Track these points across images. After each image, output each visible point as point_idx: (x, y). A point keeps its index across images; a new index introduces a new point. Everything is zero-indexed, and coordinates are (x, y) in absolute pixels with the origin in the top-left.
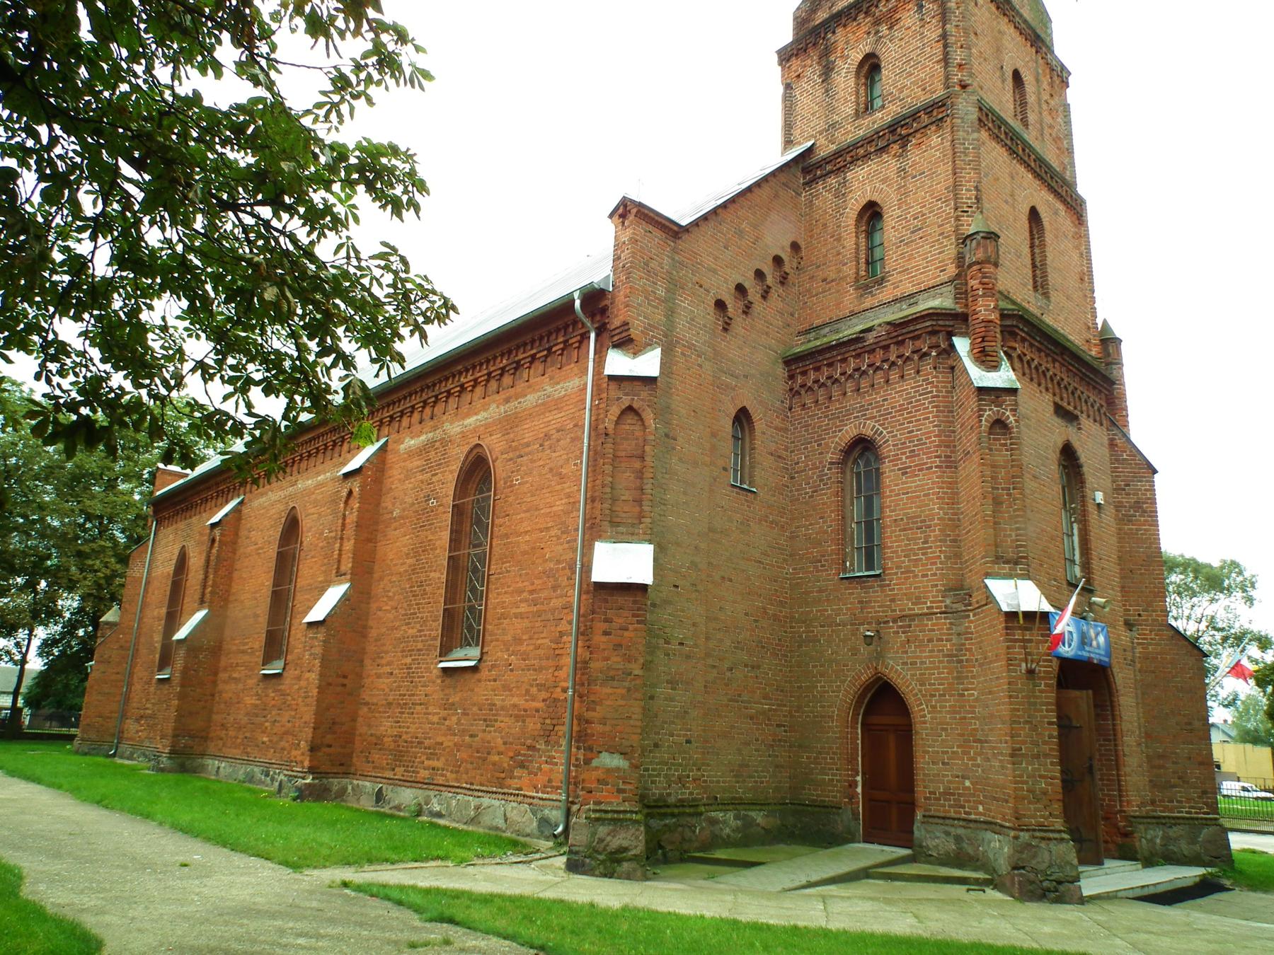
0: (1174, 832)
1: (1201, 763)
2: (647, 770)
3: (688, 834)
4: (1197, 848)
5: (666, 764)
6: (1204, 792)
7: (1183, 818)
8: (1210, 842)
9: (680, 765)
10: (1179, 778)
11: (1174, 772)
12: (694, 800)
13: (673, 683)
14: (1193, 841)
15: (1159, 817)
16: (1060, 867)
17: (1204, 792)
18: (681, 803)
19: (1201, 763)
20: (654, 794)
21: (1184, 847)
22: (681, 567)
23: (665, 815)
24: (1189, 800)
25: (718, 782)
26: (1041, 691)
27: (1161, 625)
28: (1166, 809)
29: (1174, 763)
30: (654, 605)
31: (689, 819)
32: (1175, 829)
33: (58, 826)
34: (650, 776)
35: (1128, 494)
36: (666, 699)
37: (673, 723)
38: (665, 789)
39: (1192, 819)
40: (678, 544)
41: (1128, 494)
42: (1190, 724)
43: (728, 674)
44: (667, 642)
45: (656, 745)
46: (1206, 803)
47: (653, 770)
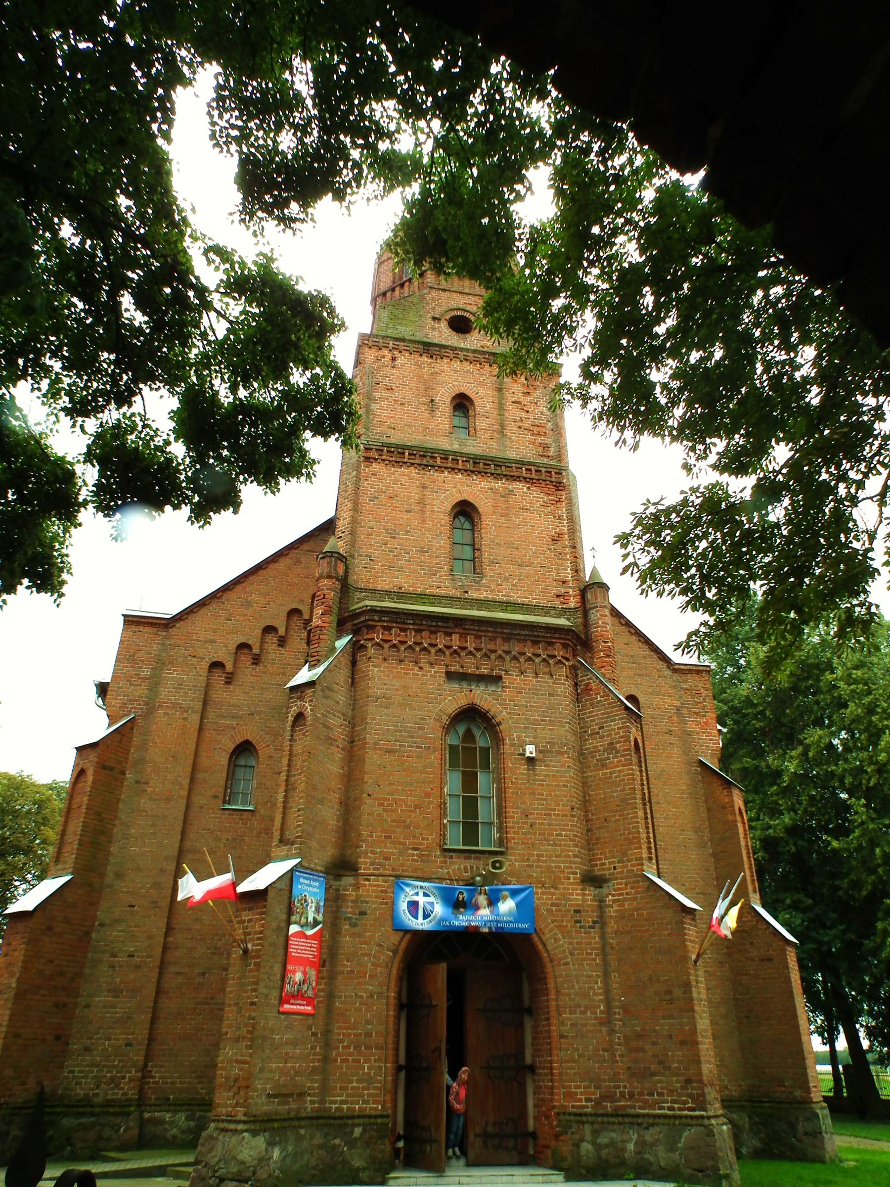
0: (649, 1136)
1: (683, 1043)
2: (73, 1072)
3: (107, 1132)
4: (676, 1156)
5: (97, 1066)
6: (688, 1081)
7: (665, 1116)
8: (692, 1148)
9: (115, 1067)
10: (660, 1062)
11: (654, 1056)
12: (126, 1100)
13: (115, 992)
14: (672, 1147)
15: (637, 1116)
16: (226, 1162)
17: (688, 1081)
18: (109, 1103)
19: (683, 1043)
20: (78, 1094)
21: (662, 1156)
22: (141, 888)
23: (83, 1114)
24: (671, 1092)
25: (172, 1083)
26: (250, 971)
27: (638, 876)
28: (646, 1104)
29: (654, 1044)
30: (102, 925)
31: (112, 1119)
32: (652, 1130)
33: (220, 1150)
34: (74, 1077)
35: (603, 737)
36: (104, 1007)
37: (111, 1028)
38: (91, 1089)
39: (675, 1117)
40: (139, 869)
41: (603, 737)
42: (669, 992)
43: (198, 980)
44: (114, 955)
45: (87, 1049)
46: (690, 1096)
47: (79, 1072)
